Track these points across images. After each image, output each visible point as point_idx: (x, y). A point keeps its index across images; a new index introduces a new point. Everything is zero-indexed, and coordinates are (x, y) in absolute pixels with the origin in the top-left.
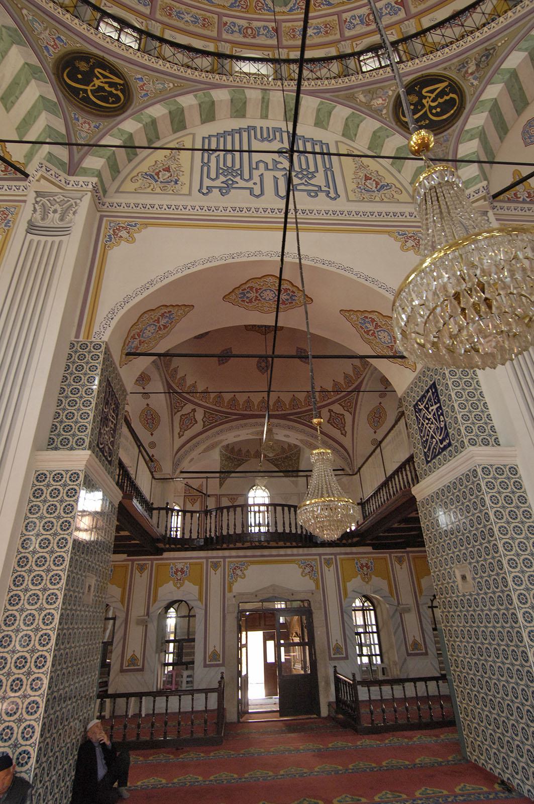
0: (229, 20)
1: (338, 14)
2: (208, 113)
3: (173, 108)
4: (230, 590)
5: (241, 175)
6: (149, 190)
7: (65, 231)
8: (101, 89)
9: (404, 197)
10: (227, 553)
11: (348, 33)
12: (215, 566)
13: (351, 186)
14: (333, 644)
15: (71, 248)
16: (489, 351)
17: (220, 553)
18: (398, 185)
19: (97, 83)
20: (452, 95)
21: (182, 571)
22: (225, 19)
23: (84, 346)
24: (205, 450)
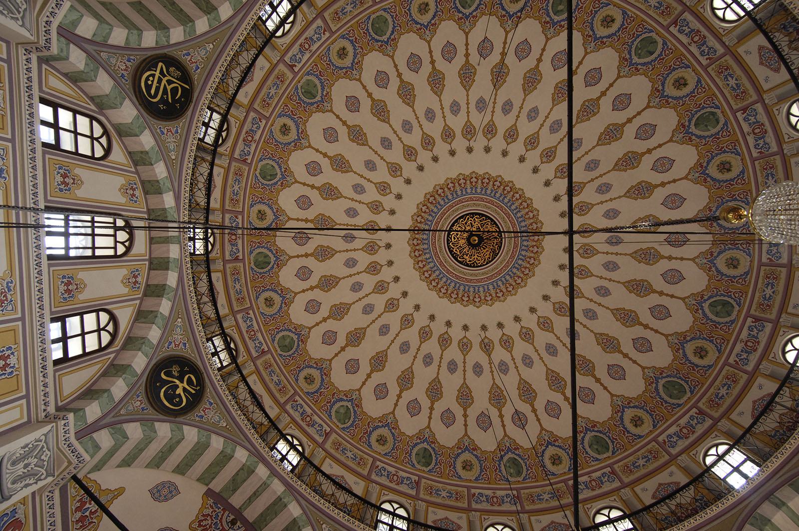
0: (262, 124)
3: (229, 451)
11: (319, 22)
22: (473, 491)
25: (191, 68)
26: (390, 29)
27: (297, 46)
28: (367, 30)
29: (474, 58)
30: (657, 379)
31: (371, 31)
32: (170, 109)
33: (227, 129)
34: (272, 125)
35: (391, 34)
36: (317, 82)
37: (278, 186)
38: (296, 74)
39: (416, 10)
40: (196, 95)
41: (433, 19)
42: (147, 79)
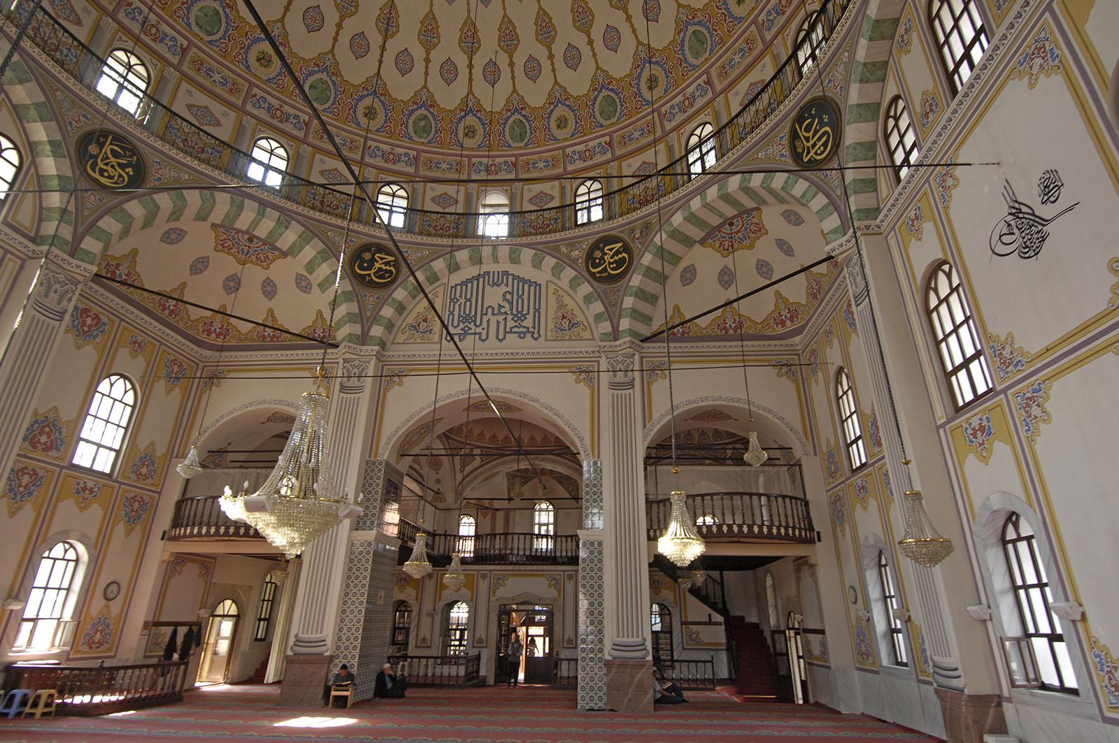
1: (563, 149)
2: (454, 267)
4: (494, 595)
5: (475, 321)
6: (412, 341)
7: (360, 389)
8: (380, 269)
9: (586, 334)
10: (493, 567)
11: (668, 126)
12: (484, 577)
13: (551, 326)
14: (567, 637)
15: (364, 400)
17: (488, 567)
18: (585, 323)
19: (377, 265)
20: (624, 254)
21: (982, 429)
23: (374, 463)
24: (484, 481)
25: (785, 141)
26: (598, 102)
27: (696, 106)
28: (622, 105)
29: (503, 60)
30: (326, 70)
31: (619, 104)
32: (822, 111)
33: (800, 30)
34: (753, 9)
35: (597, 96)
36: (687, 52)
37: (338, 80)
38: (707, 72)
39: (569, 122)
40: (794, 113)
41: (552, 110)
42: (822, 152)
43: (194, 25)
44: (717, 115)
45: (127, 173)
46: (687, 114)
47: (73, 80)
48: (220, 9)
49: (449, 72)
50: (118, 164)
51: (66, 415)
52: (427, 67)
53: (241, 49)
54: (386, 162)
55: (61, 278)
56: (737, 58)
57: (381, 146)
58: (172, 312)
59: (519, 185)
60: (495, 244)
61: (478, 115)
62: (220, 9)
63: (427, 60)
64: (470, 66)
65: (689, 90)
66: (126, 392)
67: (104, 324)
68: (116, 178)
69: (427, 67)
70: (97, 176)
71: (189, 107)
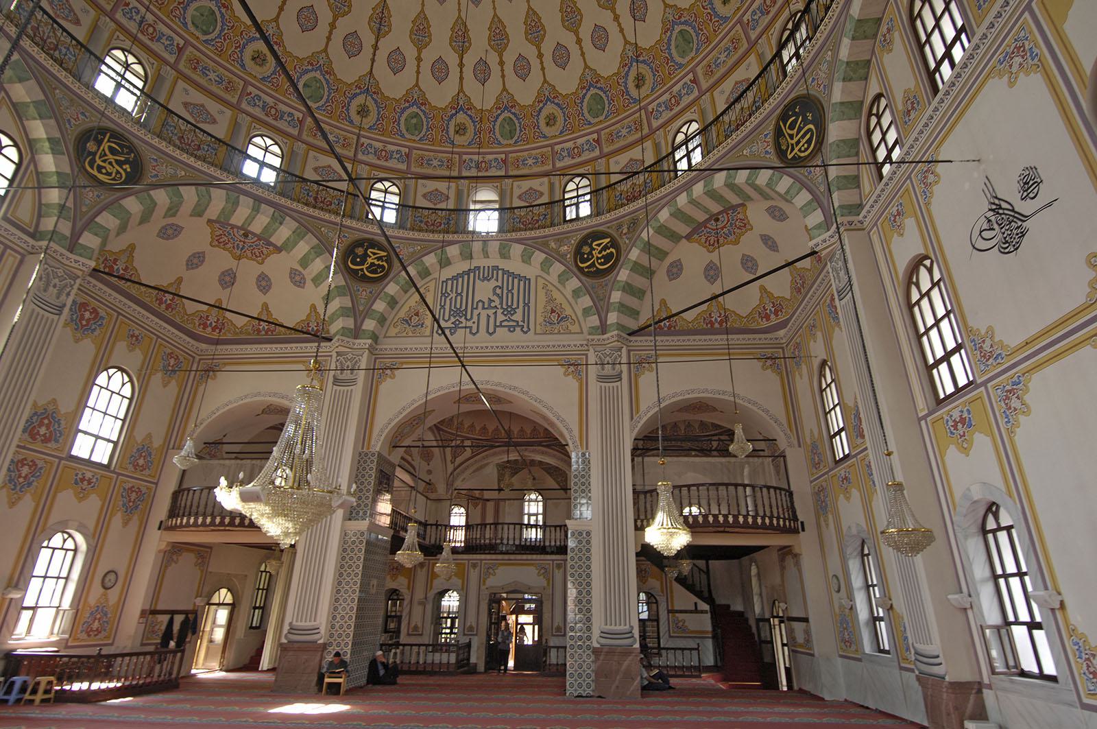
1: (552, 146)
2: (445, 262)
4: (484, 584)
5: (466, 315)
6: (404, 334)
7: (353, 382)
8: (372, 264)
9: (575, 328)
10: (483, 557)
11: (655, 124)
12: (474, 566)
13: (540, 320)
14: (556, 625)
15: (357, 392)
16: (436, 570)
17: (478, 557)
18: (574, 317)
19: (369, 260)
20: (612, 250)
23: (366, 455)
24: (474, 472)
25: (770, 139)
26: (586, 100)
27: (683, 104)
28: (610, 103)
29: (493, 59)
31: (606, 102)
32: (806, 109)
33: (785, 29)
34: (738, 9)
35: (585, 94)
36: (674, 51)
37: (331, 79)
38: (693, 71)
39: (558, 119)
40: (778, 111)
41: (541, 108)
42: (806, 150)
43: (190, 25)
44: (703, 113)
45: (125, 170)
46: (674, 112)
47: (71, 79)
48: (216, 9)
49: (440, 71)
50: (116, 160)
51: (65, 407)
52: (418, 66)
53: (236, 48)
54: (379, 159)
55: (60, 272)
56: (722, 57)
57: (374, 143)
58: (168, 307)
59: (508, 181)
60: (486, 239)
61: (469, 113)
62: (216, 9)
63: (419, 59)
64: (461, 65)
65: (676, 89)
66: (123, 384)
67: (102, 318)
68: (114, 175)
69: (418, 66)
70: (95, 172)
71: (186, 105)
